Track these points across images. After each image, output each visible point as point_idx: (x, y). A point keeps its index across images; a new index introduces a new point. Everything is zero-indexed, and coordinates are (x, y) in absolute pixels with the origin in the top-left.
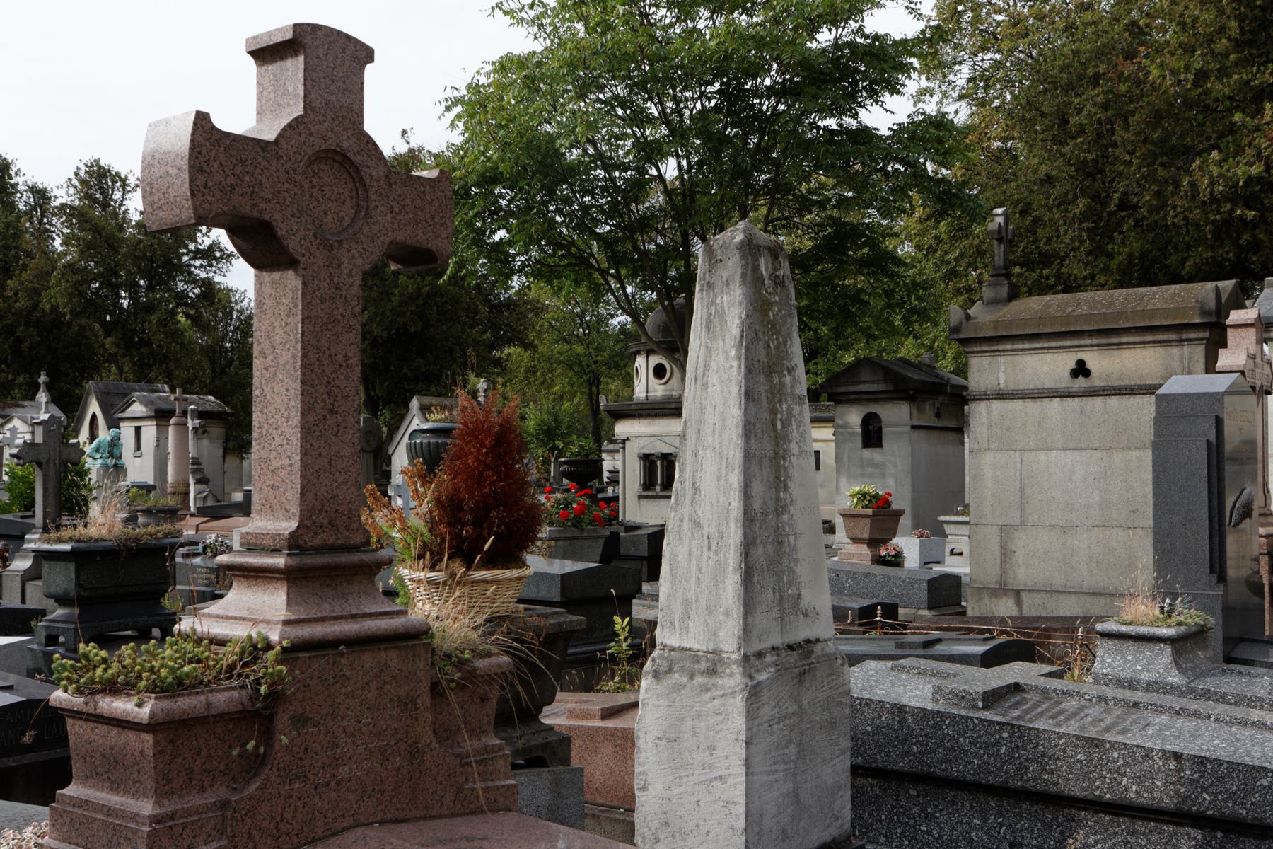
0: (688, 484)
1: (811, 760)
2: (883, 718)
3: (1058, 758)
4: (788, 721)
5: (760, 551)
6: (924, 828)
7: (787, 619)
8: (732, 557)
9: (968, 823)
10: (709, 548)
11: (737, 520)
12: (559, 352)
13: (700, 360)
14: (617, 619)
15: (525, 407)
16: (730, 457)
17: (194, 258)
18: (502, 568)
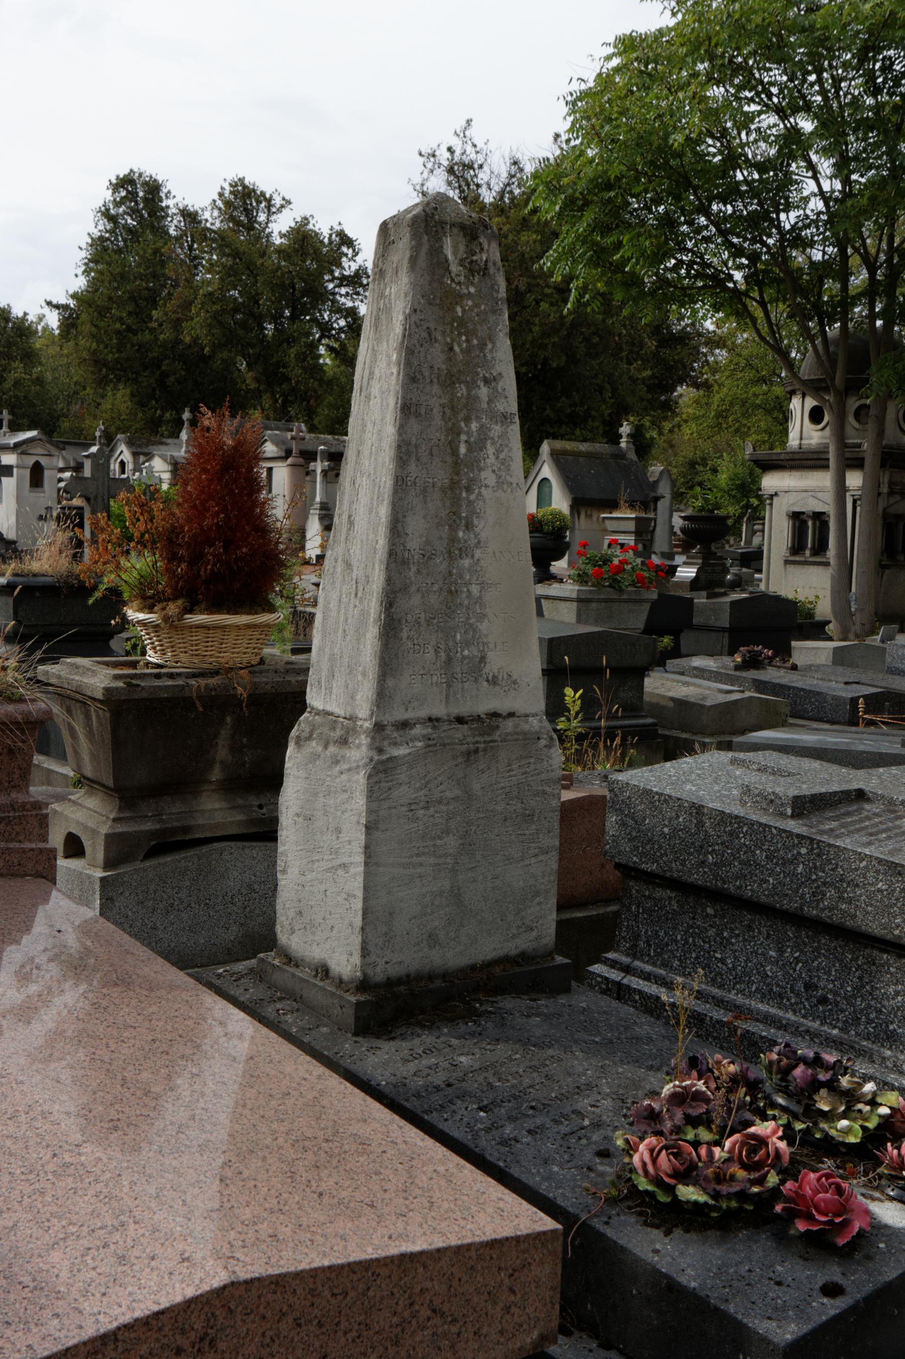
0: (345, 517)
2: (681, 819)
3: (857, 885)
4: (444, 808)
5: (416, 600)
8: (373, 606)
9: (763, 954)
10: (356, 595)
11: (381, 561)
14: (569, 691)
15: (718, 458)
16: (382, 484)
17: (340, 286)
18: (228, 613)
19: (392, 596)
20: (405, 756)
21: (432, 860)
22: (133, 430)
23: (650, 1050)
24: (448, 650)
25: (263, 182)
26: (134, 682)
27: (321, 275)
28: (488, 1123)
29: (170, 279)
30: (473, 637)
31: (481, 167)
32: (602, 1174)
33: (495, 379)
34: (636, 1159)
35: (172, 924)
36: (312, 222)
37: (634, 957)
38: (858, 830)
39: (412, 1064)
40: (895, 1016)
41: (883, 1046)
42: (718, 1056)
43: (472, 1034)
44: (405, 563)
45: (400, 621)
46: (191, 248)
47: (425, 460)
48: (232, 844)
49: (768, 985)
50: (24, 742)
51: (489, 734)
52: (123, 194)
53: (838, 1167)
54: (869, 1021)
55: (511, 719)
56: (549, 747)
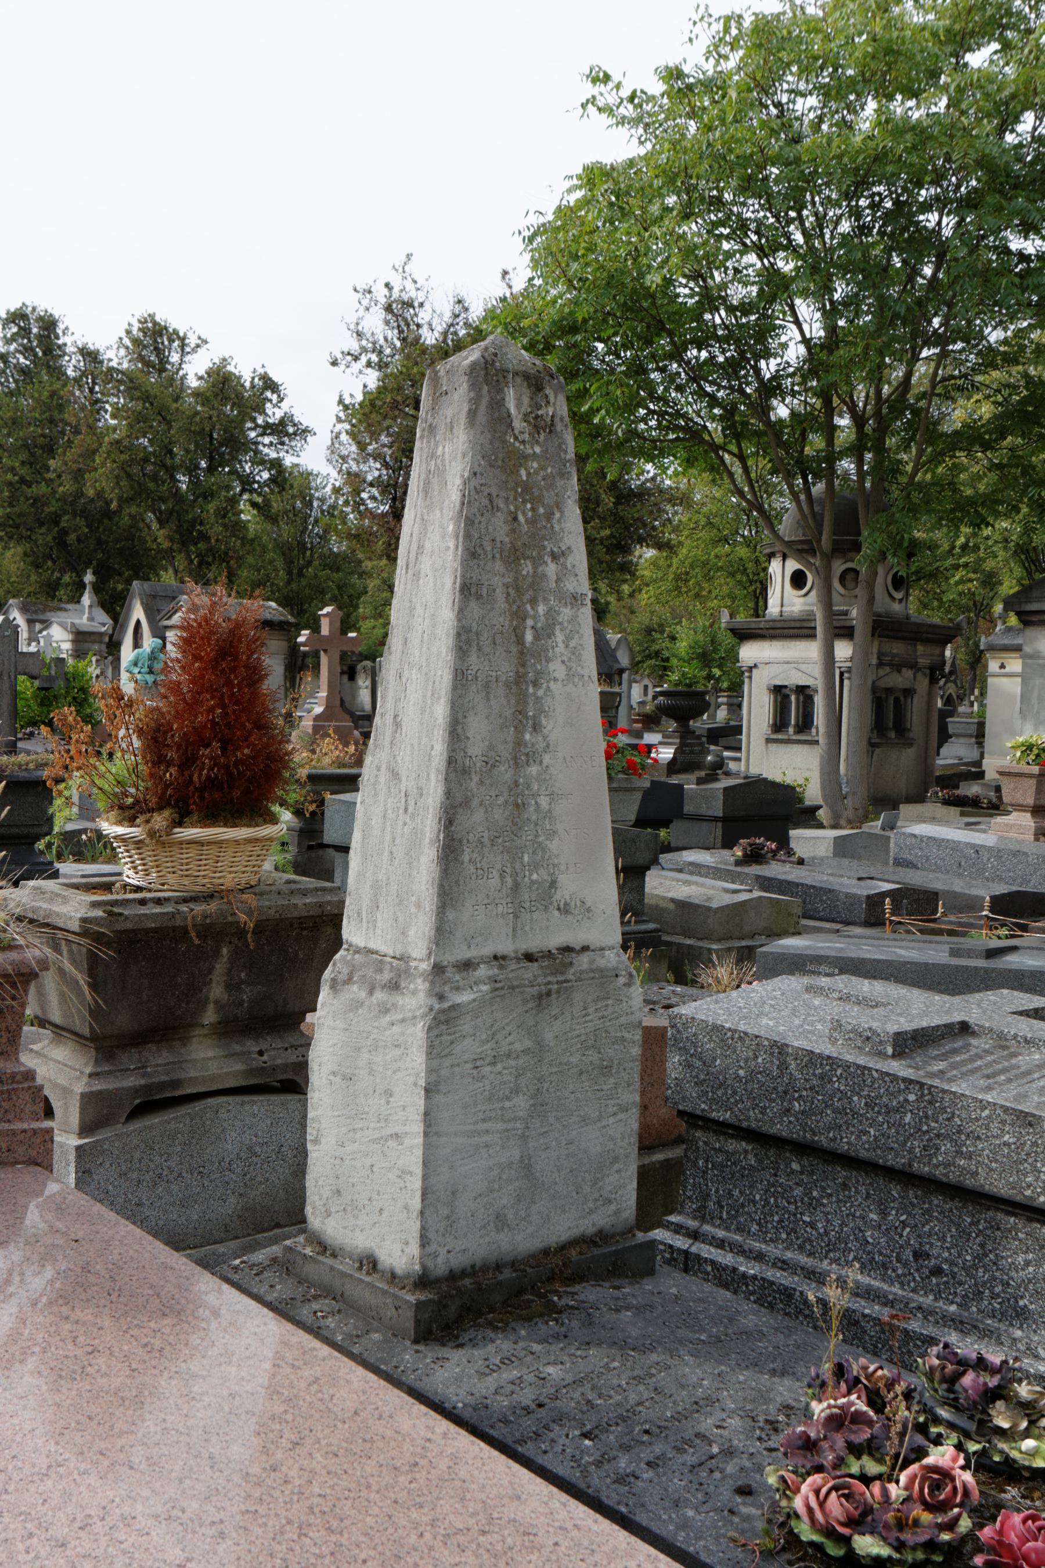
0: (389, 718)
1: (557, 1118)
2: (760, 1060)
3: (978, 1138)
4: (512, 1063)
5: (478, 816)
6: (807, 1219)
7: (525, 916)
8: (429, 825)
10: (406, 810)
11: (438, 770)
12: (717, 556)
13: (414, 538)
16: (438, 679)
17: (263, 434)
18: (225, 825)
19: (452, 812)
20: (469, 1003)
21: (500, 1126)
22: (25, 593)
23: (766, 1348)
24: (515, 875)
25: (176, 322)
26: (116, 910)
27: (243, 421)
28: (597, 1455)
29: (67, 424)
30: (543, 857)
31: (421, 305)
32: (748, 1518)
33: (563, 554)
34: (798, 1503)
35: (160, 1198)
36: (233, 363)
37: (703, 1220)
38: (973, 1071)
39: (490, 1379)
40: (1026, 1290)
41: (1011, 1325)
42: (862, 1361)
43: (557, 1337)
44: (466, 772)
45: (460, 841)
46: (91, 390)
47: (486, 649)
48: (230, 1099)
49: (869, 1253)
50: (13, 998)
51: (562, 973)
52: (15, 330)
53: (1023, 1497)
54: (994, 1296)
55: (586, 954)
56: (628, 985)
